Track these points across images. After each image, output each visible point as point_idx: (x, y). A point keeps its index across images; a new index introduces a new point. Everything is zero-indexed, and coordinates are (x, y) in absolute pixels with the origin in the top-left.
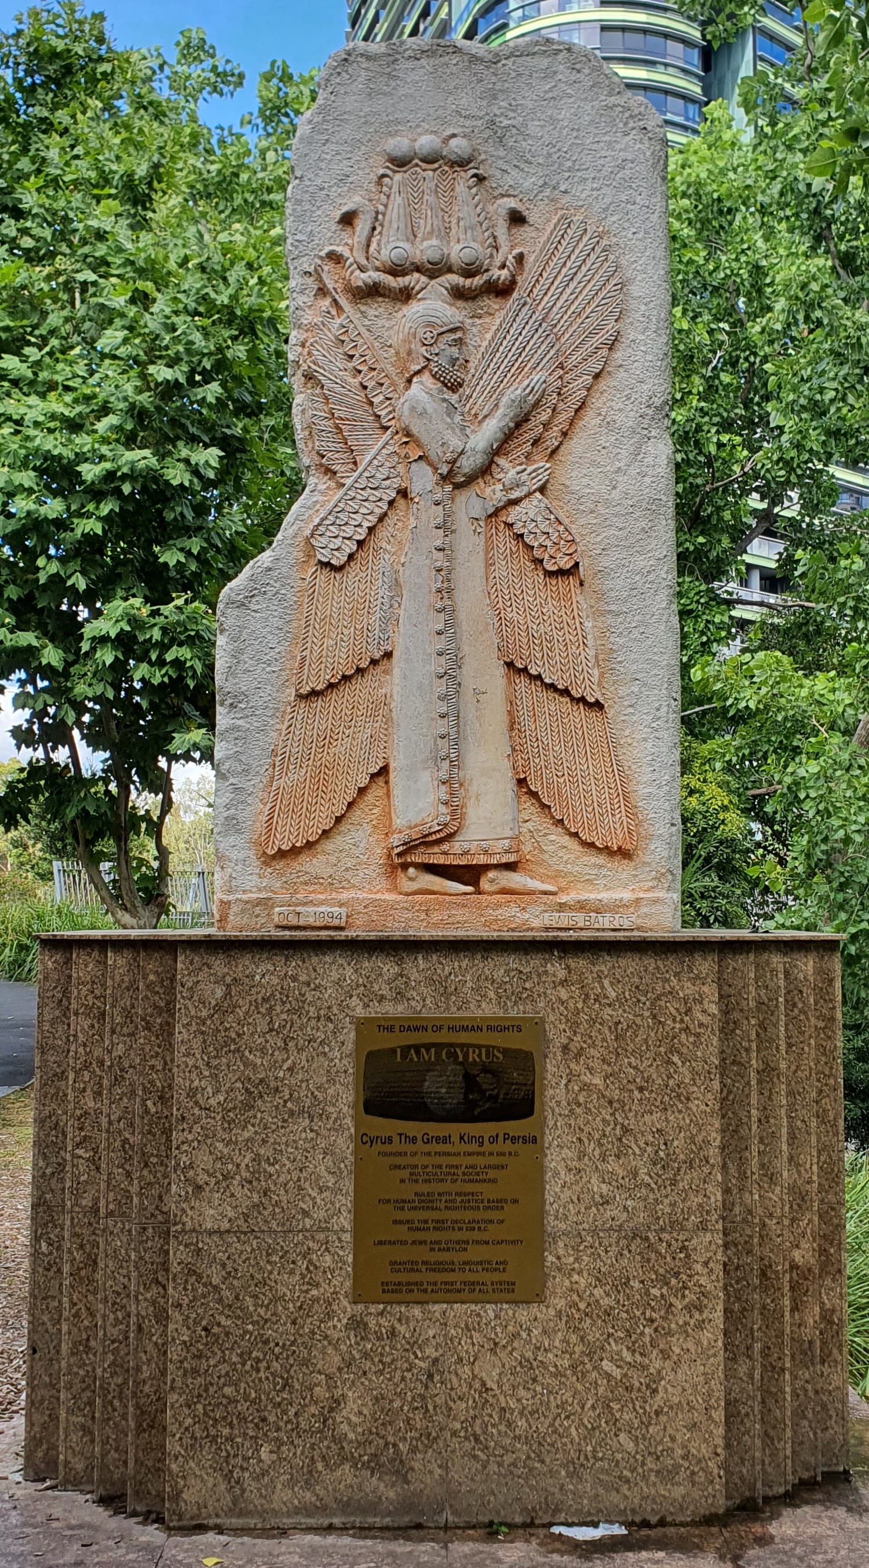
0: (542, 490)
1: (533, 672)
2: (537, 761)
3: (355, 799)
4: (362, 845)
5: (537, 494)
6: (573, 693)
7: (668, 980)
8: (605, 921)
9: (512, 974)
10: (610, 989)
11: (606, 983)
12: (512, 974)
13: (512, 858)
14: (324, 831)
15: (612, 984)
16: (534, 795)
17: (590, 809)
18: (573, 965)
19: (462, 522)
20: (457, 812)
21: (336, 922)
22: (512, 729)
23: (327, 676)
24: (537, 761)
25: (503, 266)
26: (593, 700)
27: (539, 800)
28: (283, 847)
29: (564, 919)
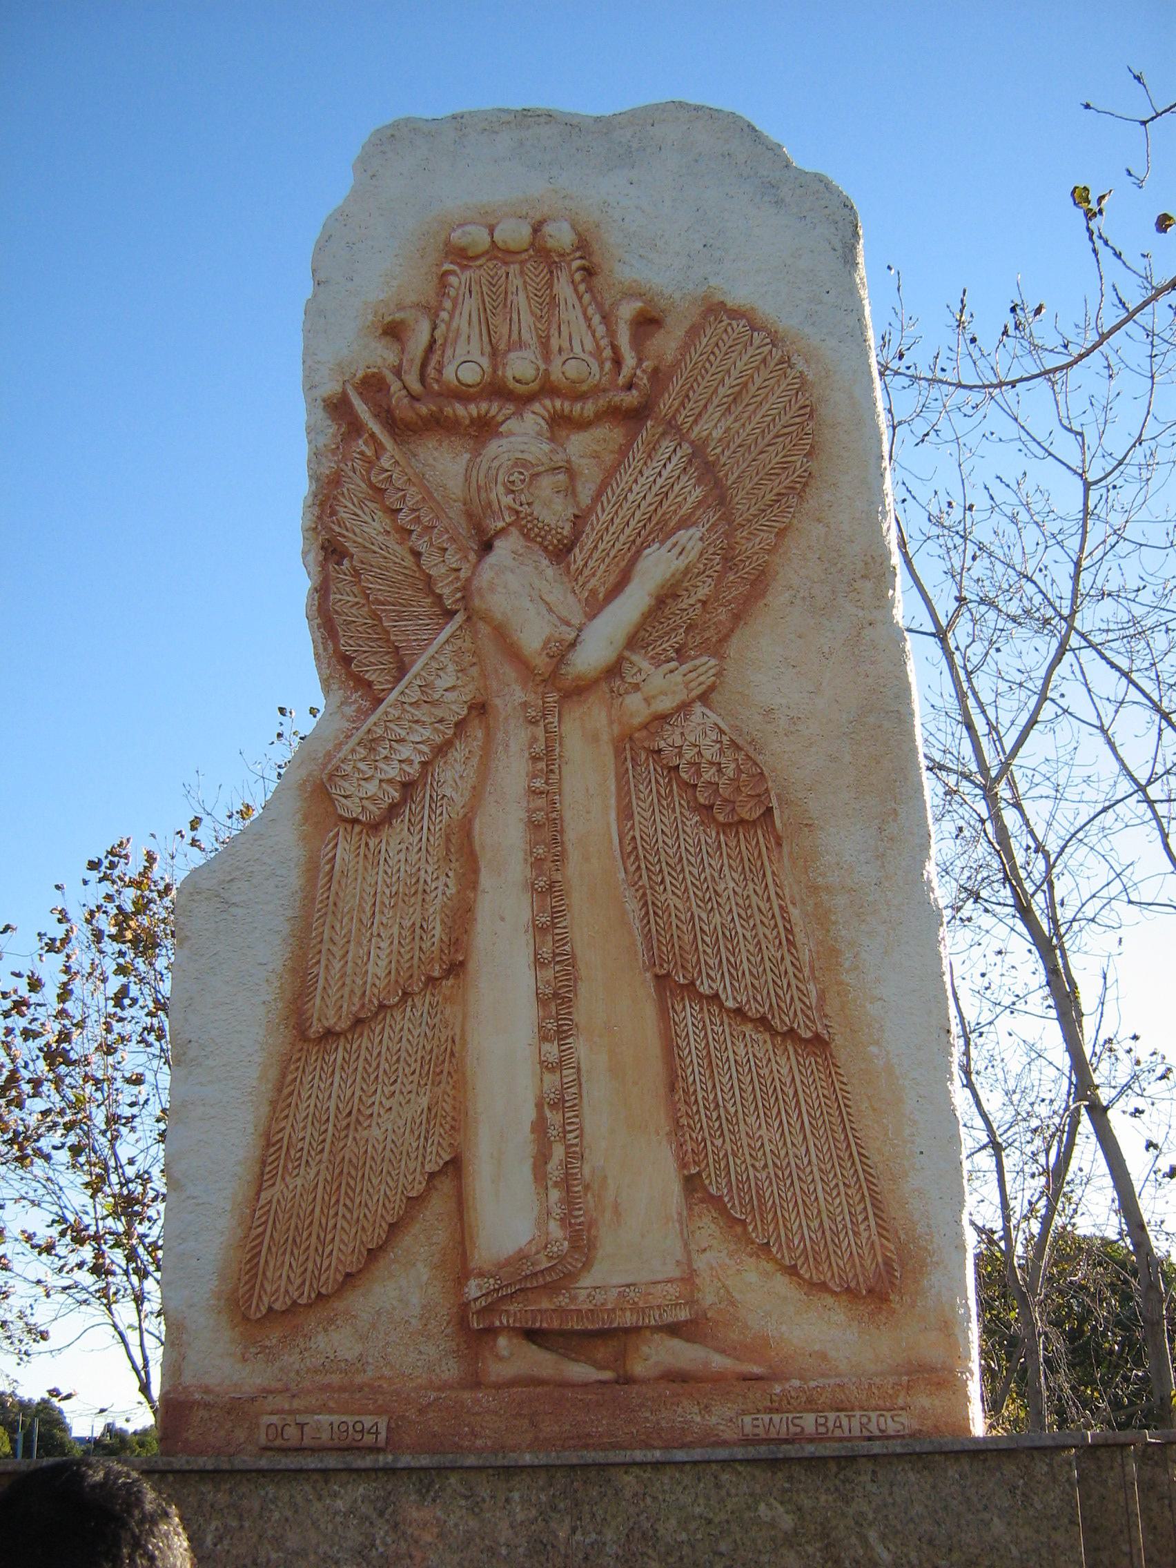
0: (704, 698)
1: (705, 989)
2: (719, 1142)
3: (401, 1219)
4: (406, 1292)
5: (698, 708)
6: (776, 1023)
7: (987, 1524)
8: (852, 1424)
9: (693, 1526)
10: (880, 1549)
11: (872, 1535)
12: (693, 1526)
13: (683, 1315)
14: (348, 1275)
15: (883, 1538)
16: (715, 1201)
17: (816, 1224)
18: (807, 1503)
19: (575, 746)
20: (582, 1242)
21: (369, 1439)
22: (672, 1089)
23: (351, 1007)
24: (719, 1142)
25: (630, 386)
26: (809, 1035)
27: (724, 1211)
28: (277, 1306)
29: (780, 1424)
